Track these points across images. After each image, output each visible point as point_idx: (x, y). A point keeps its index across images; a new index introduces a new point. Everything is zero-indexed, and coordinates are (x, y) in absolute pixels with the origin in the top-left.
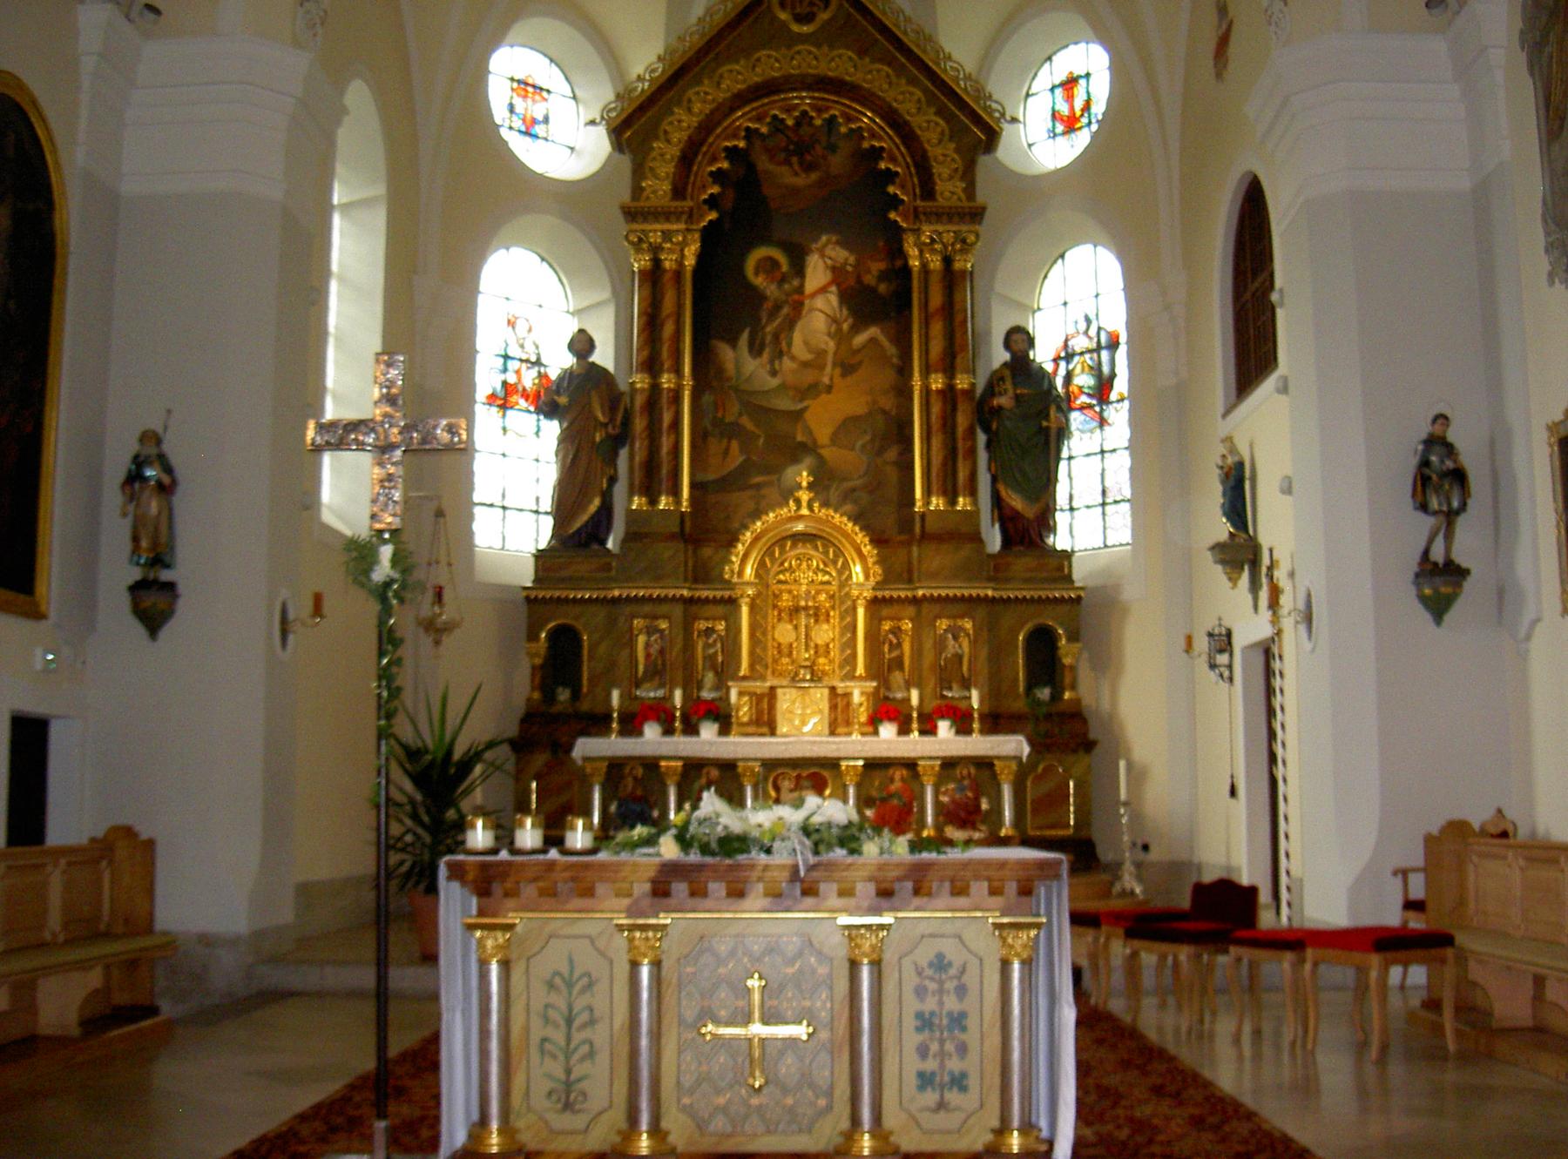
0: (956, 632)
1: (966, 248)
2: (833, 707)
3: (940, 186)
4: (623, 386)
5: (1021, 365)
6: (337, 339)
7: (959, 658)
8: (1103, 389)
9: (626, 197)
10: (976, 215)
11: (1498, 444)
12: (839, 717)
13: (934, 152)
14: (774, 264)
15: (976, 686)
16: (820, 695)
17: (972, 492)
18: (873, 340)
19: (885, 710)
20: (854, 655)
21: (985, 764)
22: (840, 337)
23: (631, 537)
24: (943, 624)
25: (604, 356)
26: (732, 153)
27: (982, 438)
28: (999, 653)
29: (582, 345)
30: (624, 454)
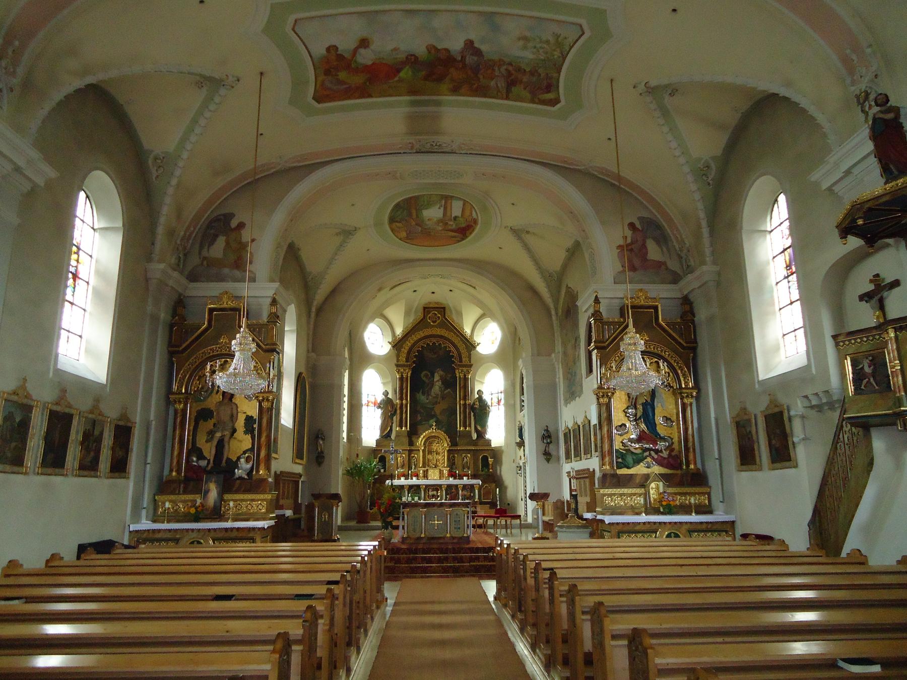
1: (469, 373)
2: (440, 473)
3: (464, 359)
4: (395, 403)
5: (480, 399)
6: (384, 642)
9: (395, 361)
10: (471, 366)
11: (557, 431)
12: (441, 475)
15: (558, 664)
16: (437, 472)
17: (470, 426)
18: (449, 392)
20: (445, 462)
21: (472, 486)
22: (441, 391)
23: (397, 436)
24: (464, 455)
25: (390, 396)
26: (418, 351)
27: (472, 414)
28: (475, 463)
29: (386, 393)
30: (395, 418)
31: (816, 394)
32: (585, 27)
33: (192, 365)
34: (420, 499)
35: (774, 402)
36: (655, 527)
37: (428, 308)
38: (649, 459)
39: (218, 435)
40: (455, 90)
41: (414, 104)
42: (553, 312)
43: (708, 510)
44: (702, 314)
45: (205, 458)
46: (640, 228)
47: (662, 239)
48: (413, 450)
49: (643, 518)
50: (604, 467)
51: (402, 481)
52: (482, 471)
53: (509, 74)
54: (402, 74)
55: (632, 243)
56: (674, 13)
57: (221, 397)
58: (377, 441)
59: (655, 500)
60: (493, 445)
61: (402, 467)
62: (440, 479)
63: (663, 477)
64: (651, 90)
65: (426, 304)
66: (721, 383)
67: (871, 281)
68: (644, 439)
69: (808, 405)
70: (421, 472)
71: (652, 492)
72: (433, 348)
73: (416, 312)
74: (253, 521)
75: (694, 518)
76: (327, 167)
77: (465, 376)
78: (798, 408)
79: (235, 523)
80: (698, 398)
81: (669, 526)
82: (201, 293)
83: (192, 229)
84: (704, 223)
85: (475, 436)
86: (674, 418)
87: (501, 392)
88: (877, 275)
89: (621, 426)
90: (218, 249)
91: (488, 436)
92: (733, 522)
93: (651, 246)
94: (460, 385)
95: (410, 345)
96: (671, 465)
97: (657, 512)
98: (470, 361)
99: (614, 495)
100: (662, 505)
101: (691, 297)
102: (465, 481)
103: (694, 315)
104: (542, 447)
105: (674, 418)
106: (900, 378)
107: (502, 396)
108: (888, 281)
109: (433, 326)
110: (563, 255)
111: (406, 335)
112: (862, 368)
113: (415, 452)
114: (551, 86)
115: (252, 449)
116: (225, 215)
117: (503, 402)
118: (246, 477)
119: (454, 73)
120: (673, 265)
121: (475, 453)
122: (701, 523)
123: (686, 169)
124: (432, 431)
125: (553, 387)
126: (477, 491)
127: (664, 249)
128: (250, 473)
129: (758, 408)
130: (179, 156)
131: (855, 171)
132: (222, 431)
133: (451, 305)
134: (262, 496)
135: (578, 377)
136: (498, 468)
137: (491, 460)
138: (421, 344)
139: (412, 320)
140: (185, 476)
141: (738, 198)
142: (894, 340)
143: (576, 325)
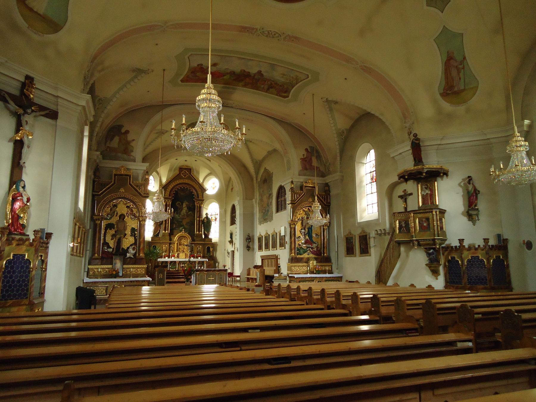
0: (199, 247)
1: (202, 204)
5: (207, 217)
7: (199, 250)
8: (216, 219)
10: (204, 200)
13: (199, 193)
14: (179, 204)
16: (184, 254)
17: (201, 231)
19: (192, 256)
21: (203, 262)
26: (175, 191)
31: (381, 230)
32: (310, 76)
33: (105, 202)
34: (204, 268)
35: (363, 231)
36: (313, 279)
37: (182, 168)
38: (309, 251)
39: (118, 236)
40: (245, 86)
41: (223, 87)
42: (255, 179)
43: (331, 272)
44: (333, 192)
45: (111, 248)
46: (310, 151)
47: (319, 157)
48: (172, 243)
49: (309, 275)
50: (292, 255)
51: (167, 259)
52: (207, 254)
53: (271, 84)
54: (225, 77)
55: (306, 158)
56: (345, 80)
57: (118, 218)
58: (152, 238)
59: (312, 268)
60: (213, 241)
61: (166, 252)
62: (185, 258)
63: (316, 259)
64: (327, 101)
65: (181, 166)
66: (340, 220)
67: (403, 192)
68: (307, 243)
69: (377, 233)
70: (176, 254)
71: (311, 265)
72: (183, 190)
73: (175, 170)
74: (140, 277)
75: (327, 275)
76: (171, 107)
77: (200, 205)
78: (373, 234)
79: (134, 278)
80: (329, 227)
81: (318, 278)
82: (108, 165)
83: (432, 251)
84: (338, 155)
85: (203, 236)
86: (319, 234)
87: (217, 215)
88: (405, 190)
89: (299, 237)
90: (115, 143)
91: (210, 237)
92: (342, 277)
93: (314, 159)
94: (197, 210)
95: (171, 187)
96: (317, 254)
97: (312, 273)
98: (203, 197)
99: (296, 266)
100: (316, 270)
101: (329, 184)
102: (199, 259)
103: (330, 192)
104: (246, 243)
105: (319, 234)
106: (413, 229)
107: (218, 217)
108: (409, 193)
109: (184, 178)
110: (265, 153)
111: (168, 183)
112: (402, 225)
113: (173, 244)
114: (287, 91)
115: (135, 244)
116: (119, 126)
117: (218, 219)
118: (133, 257)
119: (248, 80)
120: (322, 169)
121: (204, 245)
122: (330, 277)
123: (334, 132)
124: (182, 233)
125: (252, 215)
126: (205, 264)
127: (319, 161)
128: (135, 255)
129: (357, 233)
130: (112, 100)
131: (403, 154)
132: (120, 235)
133: (194, 168)
134: (142, 266)
135: (270, 213)
136: (215, 253)
137: (211, 249)
138: (177, 187)
139: (172, 174)
140: (102, 256)
141: (355, 149)
142: (413, 217)
143: (270, 188)
